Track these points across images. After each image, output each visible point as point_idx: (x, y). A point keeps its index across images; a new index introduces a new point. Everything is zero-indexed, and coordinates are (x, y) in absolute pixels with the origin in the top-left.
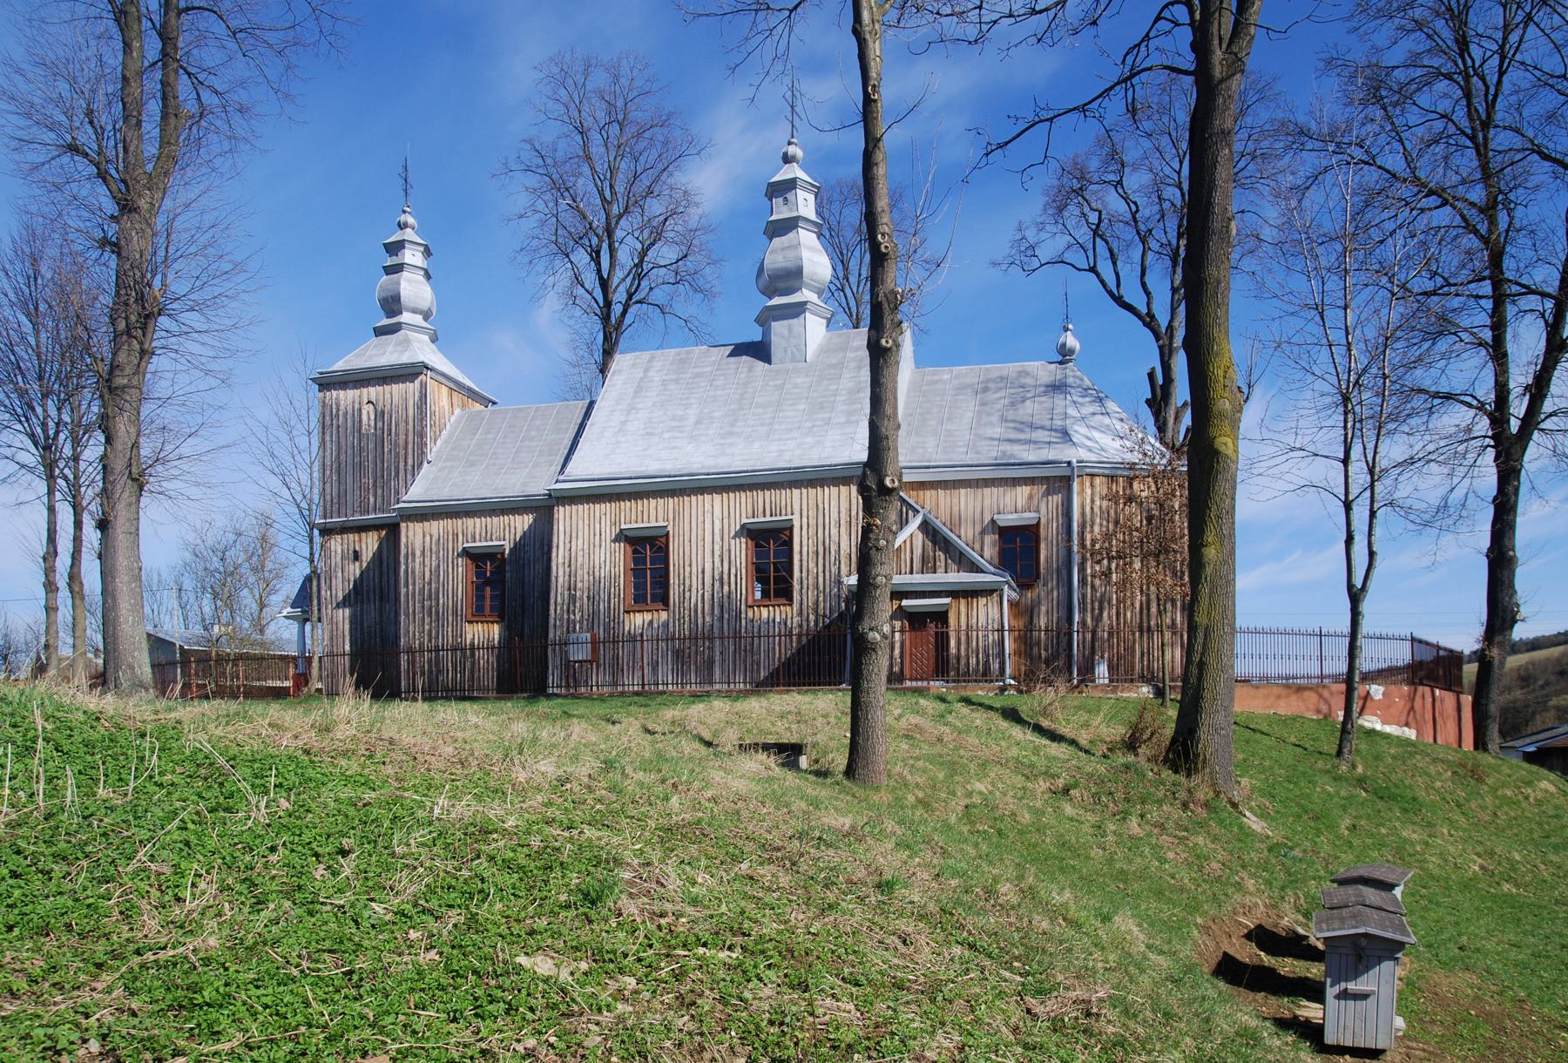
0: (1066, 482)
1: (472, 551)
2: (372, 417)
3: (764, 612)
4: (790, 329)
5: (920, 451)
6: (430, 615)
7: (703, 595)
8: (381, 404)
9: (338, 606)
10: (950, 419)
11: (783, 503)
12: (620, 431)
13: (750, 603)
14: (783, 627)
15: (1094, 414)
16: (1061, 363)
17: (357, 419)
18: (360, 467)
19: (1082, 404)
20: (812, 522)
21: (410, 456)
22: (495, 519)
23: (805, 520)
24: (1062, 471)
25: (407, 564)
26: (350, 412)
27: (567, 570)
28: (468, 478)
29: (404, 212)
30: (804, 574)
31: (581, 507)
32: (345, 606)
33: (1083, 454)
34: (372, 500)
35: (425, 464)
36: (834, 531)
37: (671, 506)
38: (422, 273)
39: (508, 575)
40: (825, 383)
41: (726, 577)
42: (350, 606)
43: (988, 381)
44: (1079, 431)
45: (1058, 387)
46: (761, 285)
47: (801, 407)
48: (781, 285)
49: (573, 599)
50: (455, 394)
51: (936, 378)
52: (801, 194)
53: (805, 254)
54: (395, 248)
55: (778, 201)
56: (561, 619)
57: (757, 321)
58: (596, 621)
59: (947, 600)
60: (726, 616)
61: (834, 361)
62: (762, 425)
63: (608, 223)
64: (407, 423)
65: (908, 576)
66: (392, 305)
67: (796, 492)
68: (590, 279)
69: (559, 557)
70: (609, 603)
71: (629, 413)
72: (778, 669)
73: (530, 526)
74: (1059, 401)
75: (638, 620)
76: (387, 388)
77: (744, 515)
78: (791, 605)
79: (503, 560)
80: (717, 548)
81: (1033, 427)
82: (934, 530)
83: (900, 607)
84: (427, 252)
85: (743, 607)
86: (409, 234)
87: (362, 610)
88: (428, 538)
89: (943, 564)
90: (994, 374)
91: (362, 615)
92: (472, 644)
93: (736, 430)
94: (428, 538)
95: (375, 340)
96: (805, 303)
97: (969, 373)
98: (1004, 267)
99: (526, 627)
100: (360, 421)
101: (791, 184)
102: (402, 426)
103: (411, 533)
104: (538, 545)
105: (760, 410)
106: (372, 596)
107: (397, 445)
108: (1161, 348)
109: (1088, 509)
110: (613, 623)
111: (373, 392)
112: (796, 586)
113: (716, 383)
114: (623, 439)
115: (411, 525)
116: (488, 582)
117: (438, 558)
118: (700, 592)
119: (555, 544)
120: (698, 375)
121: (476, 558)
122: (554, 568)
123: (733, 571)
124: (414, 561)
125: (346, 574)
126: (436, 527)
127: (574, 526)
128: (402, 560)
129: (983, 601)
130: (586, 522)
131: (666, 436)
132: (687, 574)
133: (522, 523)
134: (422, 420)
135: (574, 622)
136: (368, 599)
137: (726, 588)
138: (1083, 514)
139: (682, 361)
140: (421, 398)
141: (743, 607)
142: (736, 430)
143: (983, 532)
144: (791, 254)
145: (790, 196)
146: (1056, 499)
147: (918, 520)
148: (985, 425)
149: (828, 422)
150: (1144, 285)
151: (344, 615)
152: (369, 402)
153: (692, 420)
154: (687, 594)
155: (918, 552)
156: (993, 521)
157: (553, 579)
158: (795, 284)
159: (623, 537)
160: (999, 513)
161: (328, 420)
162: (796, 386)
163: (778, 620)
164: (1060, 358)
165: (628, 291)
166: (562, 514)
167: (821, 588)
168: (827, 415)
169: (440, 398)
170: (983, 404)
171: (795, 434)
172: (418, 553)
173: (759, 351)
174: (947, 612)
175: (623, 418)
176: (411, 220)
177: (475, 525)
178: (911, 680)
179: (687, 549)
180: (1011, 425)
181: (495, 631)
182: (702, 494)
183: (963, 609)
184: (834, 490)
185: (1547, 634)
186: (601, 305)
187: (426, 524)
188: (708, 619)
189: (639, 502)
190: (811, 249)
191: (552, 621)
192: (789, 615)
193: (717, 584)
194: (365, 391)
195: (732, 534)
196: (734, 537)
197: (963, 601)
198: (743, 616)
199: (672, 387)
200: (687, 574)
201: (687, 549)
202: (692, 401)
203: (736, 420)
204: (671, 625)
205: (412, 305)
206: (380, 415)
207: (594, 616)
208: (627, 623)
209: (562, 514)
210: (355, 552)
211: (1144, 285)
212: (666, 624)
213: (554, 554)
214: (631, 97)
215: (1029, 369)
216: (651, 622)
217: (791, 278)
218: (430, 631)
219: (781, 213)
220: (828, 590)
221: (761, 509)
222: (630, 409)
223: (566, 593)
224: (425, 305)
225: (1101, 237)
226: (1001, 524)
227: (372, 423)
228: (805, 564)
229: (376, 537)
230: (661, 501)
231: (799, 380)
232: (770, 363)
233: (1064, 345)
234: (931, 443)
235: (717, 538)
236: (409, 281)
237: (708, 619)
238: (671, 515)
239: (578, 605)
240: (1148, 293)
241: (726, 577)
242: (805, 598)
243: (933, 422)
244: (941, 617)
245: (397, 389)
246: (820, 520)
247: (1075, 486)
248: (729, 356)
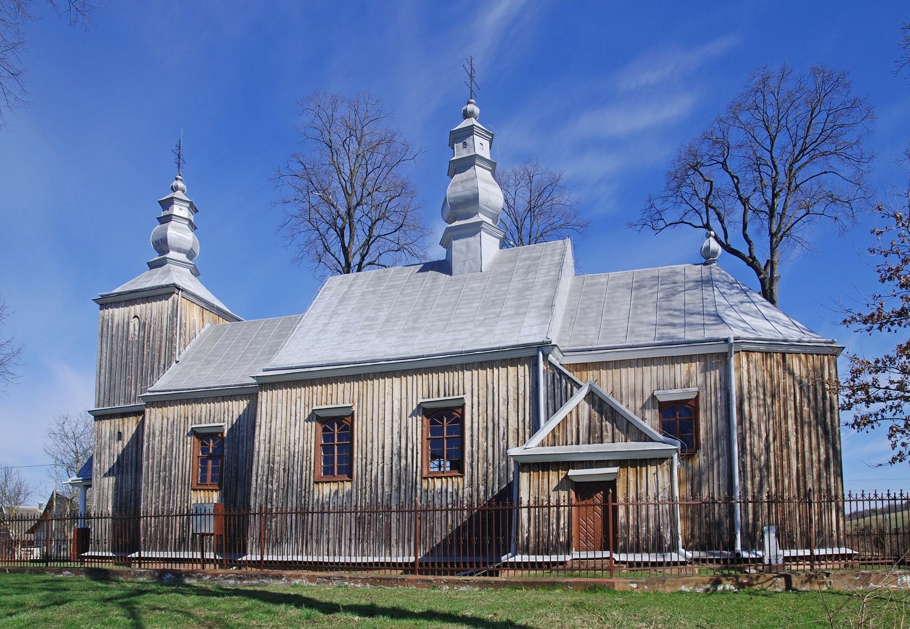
0: (724, 358)
1: (199, 431)
2: (137, 328)
3: (438, 483)
4: (468, 245)
5: (583, 337)
6: (164, 484)
7: (383, 467)
8: (143, 318)
9: (105, 476)
10: (609, 311)
11: (456, 384)
12: (321, 331)
13: (425, 475)
14: (455, 497)
15: (742, 302)
16: (705, 264)
17: (126, 330)
18: (125, 367)
19: (731, 295)
20: (482, 400)
21: (163, 357)
22: (217, 405)
23: (475, 399)
24: (722, 348)
25: (148, 441)
26: (121, 324)
27: (267, 446)
28: (203, 373)
29: (177, 179)
30: (475, 448)
31: (280, 391)
32: (110, 476)
33: (738, 333)
34: (133, 392)
35: (174, 364)
36: (503, 408)
37: (356, 390)
38: (187, 223)
39: (226, 451)
40: (497, 286)
41: (403, 451)
42: (113, 475)
43: (643, 280)
44: (731, 316)
45: (707, 282)
46: (445, 216)
47: (475, 305)
48: (461, 211)
49: (271, 470)
50: (207, 312)
51: (595, 281)
52: (477, 139)
53: (481, 185)
54: (167, 204)
55: (458, 146)
56: (261, 489)
57: (441, 244)
58: (290, 490)
59: (615, 470)
60: (403, 487)
61: (505, 270)
62: (441, 320)
63: (349, 209)
64: (162, 332)
65: (575, 446)
66: (162, 246)
67: (468, 374)
68: (336, 248)
69: (261, 434)
70: (301, 474)
71: (331, 317)
72: (451, 535)
73: (244, 411)
74: (708, 293)
75: (327, 489)
76: (149, 305)
77: (420, 396)
78: (462, 477)
79: (223, 438)
80: (396, 425)
81: (687, 313)
82: (600, 399)
83: (567, 476)
84: (193, 208)
85: (419, 478)
86: (179, 194)
87: (122, 479)
88: (165, 421)
89: (610, 434)
90: (648, 275)
91: (122, 482)
93: (417, 325)
94: (165, 421)
95: (148, 272)
96: (481, 223)
97: (624, 276)
98: (639, 227)
100: (128, 332)
101: (469, 131)
102: (158, 334)
103: (153, 417)
104: (247, 423)
105: (439, 310)
106: (130, 468)
107: (153, 348)
108: (762, 281)
109: (745, 384)
110: (304, 492)
111: (137, 309)
112: (467, 460)
113: (405, 292)
114: (323, 337)
115: (153, 410)
116: (210, 457)
117: (172, 437)
118: (381, 465)
119: (258, 424)
120: (392, 287)
121: (201, 436)
122: (257, 444)
123: (410, 446)
124: (154, 439)
125: (112, 451)
126: (171, 412)
127: (274, 408)
128: (145, 438)
129: (652, 469)
130: (285, 404)
131: (360, 332)
132: (369, 449)
133: (239, 407)
134: (173, 328)
135: (272, 491)
136: (127, 470)
137: (403, 461)
138: (741, 388)
139: (380, 278)
140: (172, 312)
141: (419, 478)
142: (417, 325)
143: (644, 407)
144: (468, 185)
145: (468, 141)
146: (714, 376)
147: (584, 392)
148: (641, 314)
149: (498, 315)
150: (745, 236)
151: (109, 483)
152: (135, 316)
153: (382, 320)
154: (369, 467)
155: (584, 422)
156: (653, 397)
157: (256, 454)
158: (471, 209)
159: (315, 417)
160: (658, 389)
161: (106, 331)
162: (472, 289)
163: (450, 490)
164: (704, 261)
165: (361, 254)
166: (264, 397)
167: (491, 461)
168: (498, 310)
169: (192, 314)
170: (637, 298)
171: (469, 326)
172: (157, 433)
173: (444, 267)
174: (615, 481)
175: (326, 321)
176: (180, 184)
177: (202, 409)
178: (579, 549)
179: (369, 426)
180: (666, 313)
181: (215, 497)
182: (383, 378)
183: (632, 479)
184: (503, 371)
186: (344, 266)
187: (164, 409)
188: (387, 489)
189: (329, 386)
190: (486, 181)
191: (253, 490)
192: (461, 486)
193: (395, 458)
194: (132, 308)
195: (410, 412)
196: (411, 416)
197: (631, 471)
198: (419, 486)
199: (369, 297)
200: (369, 449)
201: (369, 426)
202: (384, 305)
203: (418, 318)
204: (354, 495)
205: (177, 246)
206: (142, 326)
207: (288, 486)
208: (316, 492)
209: (264, 397)
210: (119, 433)
211: (745, 236)
212: (350, 494)
213: (257, 432)
214: (366, 122)
215: (678, 270)
216: (337, 492)
217: (471, 202)
218: (164, 496)
219: (460, 153)
220: (497, 462)
221: (435, 390)
222: (335, 313)
223: (266, 465)
224: (188, 247)
225: (712, 207)
226: (662, 399)
227: (137, 333)
228: (475, 438)
229: (135, 422)
230: (347, 385)
231: (475, 285)
232: (451, 274)
233: (708, 248)
234: (592, 331)
235: (396, 417)
236: (175, 228)
237: (387, 489)
238: (356, 397)
239: (275, 476)
240: (749, 242)
241: (403, 451)
242: (475, 471)
243: (594, 315)
244: (609, 486)
245: (155, 305)
246: (490, 398)
247: (733, 361)
248: (419, 271)
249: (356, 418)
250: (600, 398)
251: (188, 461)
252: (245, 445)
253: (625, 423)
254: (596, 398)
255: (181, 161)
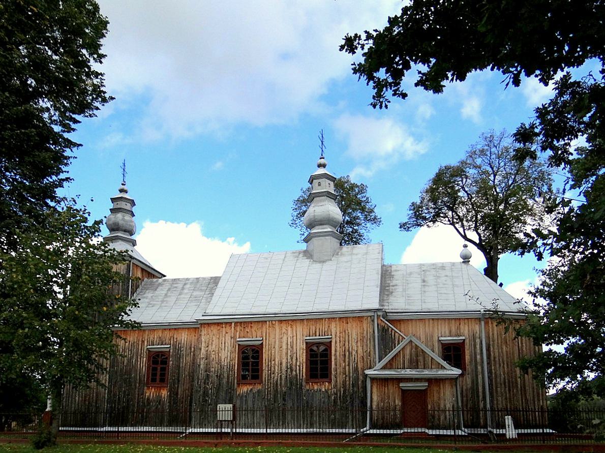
75: (245, 389)
92: (148, 399)
99: (179, 390)
167: (347, 373)
185: (408, 249)
205: (124, 228)
220: (351, 375)
249: (264, 346)
250: (416, 345)
251: (144, 369)
252: (184, 359)
253: (430, 358)
254: (414, 345)
255: (123, 167)
